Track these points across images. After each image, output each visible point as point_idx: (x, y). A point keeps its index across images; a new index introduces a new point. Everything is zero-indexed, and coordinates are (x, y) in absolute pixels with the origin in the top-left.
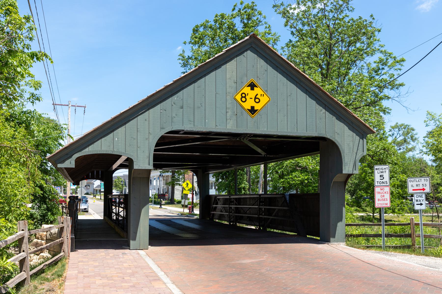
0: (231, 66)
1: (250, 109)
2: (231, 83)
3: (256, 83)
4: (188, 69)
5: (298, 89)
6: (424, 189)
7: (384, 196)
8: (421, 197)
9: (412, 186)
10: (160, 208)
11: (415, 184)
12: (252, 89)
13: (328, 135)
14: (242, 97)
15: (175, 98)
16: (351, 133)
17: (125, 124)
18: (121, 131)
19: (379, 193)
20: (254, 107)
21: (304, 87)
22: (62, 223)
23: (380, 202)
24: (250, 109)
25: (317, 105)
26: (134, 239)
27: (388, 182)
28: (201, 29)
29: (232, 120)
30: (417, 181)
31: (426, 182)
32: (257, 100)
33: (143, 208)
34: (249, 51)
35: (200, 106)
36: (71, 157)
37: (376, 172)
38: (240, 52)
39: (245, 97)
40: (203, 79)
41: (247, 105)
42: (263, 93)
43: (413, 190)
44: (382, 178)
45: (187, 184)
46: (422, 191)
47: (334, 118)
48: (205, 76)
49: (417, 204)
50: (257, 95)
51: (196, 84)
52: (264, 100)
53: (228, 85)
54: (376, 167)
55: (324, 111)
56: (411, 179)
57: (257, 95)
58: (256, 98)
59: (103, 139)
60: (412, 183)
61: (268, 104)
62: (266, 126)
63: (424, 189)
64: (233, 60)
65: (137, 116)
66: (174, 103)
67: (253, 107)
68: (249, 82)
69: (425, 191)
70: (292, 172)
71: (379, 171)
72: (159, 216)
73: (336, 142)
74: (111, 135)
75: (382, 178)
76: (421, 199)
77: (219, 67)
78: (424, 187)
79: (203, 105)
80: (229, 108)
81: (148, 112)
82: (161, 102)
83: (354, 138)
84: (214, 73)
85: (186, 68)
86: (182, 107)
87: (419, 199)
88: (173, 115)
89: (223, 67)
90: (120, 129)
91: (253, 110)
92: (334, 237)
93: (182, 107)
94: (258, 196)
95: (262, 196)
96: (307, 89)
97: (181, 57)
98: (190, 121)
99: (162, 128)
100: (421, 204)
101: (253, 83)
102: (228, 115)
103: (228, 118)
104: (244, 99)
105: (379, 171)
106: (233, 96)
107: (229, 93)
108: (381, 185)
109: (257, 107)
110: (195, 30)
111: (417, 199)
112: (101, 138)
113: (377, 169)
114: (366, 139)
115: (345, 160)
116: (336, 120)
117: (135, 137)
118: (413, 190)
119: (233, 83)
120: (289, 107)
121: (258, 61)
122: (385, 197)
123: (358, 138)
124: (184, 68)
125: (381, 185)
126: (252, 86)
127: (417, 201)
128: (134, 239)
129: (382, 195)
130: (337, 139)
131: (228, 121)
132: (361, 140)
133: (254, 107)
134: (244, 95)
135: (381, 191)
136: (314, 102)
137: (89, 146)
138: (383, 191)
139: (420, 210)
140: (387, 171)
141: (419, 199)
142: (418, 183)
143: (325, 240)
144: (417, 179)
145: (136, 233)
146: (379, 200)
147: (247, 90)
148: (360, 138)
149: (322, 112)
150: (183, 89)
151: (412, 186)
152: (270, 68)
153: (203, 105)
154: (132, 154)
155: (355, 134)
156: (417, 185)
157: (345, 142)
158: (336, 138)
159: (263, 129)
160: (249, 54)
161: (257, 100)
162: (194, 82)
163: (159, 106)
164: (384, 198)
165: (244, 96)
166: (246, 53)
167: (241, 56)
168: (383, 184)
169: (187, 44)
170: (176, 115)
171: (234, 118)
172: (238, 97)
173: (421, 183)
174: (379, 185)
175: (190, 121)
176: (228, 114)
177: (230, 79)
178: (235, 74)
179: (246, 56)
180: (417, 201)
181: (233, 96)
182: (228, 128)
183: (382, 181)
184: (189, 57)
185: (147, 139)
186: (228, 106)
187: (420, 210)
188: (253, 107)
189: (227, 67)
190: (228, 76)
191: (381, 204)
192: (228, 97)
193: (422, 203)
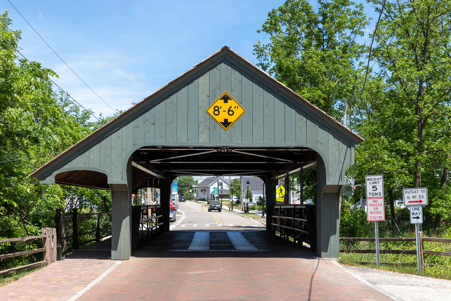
0: (203, 80)
2: (203, 97)
3: (229, 95)
5: (275, 98)
7: (377, 208)
8: (418, 209)
9: (408, 198)
10: (262, 217)
11: (411, 195)
12: (226, 102)
13: (309, 145)
14: (215, 110)
15: (147, 115)
17: (100, 142)
18: (96, 149)
19: (372, 205)
22: (45, 234)
23: (373, 215)
25: (297, 114)
26: (116, 249)
30: (414, 192)
31: (423, 194)
32: (231, 113)
33: (123, 220)
36: (51, 174)
37: (368, 182)
39: (218, 110)
40: (175, 95)
41: (220, 118)
43: (409, 202)
44: (375, 189)
45: (281, 190)
46: (419, 203)
47: (317, 126)
48: (177, 91)
49: (413, 218)
50: (231, 107)
51: (168, 100)
52: (238, 112)
53: (200, 100)
54: (368, 178)
55: (305, 119)
56: (407, 190)
57: (231, 107)
58: (229, 111)
60: (408, 195)
61: (243, 115)
62: (241, 138)
63: (421, 201)
64: (206, 75)
66: (146, 120)
67: (226, 120)
68: (222, 95)
69: (422, 203)
71: (371, 182)
72: (238, 227)
73: (318, 152)
75: (375, 189)
77: (192, 82)
78: (421, 199)
79: (175, 120)
81: (121, 130)
82: (133, 120)
83: (340, 147)
84: (186, 88)
86: (154, 124)
87: (415, 212)
90: (95, 147)
91: (226, 123)
92: (326, 251)
93: (154, 124)
94: (293, 207)
95: (297, 207)
98: (162, 137)
99: (135, 145)
102: (201, 128)
103: (200, 132)
104: (216, 113)
105: (371, 182)
106: (205, 110)
108: (374, 196)
109: (231, 119)
111: (414, 212)
112: (78, 156)
113: (368, 179)
114: (354, 147)
115: (328, 171)
116: (319, 129)
117: (109, 154)
118: (409, 202)
119: (206, 97)
120: (265, 118)
121: (232, 73)
122: (379, 210)
123: (345, 147)
125: (374, 196)
126: (226, 99)
127: (413, 214)
128: (116, 249)
129: (376, 207)
130: (320, 150)
131: (200, 135)
132: (349, 149)
134: (216, 108)
135: (374, 203)
137: (67, 163)
138: (376, 203)
139: (417, 224)
141: (415, 212)
142: (414, 195)
143: (314, 253)
145: (117, 244)
146: (371, 213)
147: (220, 103)
148: (348, 147)
149: (302, 122)
151: (408, 198)
152: (245, 79)
153: (175, 120)
154: (106, 170)
155: (341, 143)
156: (413, 197)
157: (329, 152)
159: (237, 142)
160: (223, 66)
161: (231, 113)
162: (166, 98)
163: (131, 124)
164: (377, 211)
165: (217, 110)
166: (219, 66)
167: (214, 70)
168: (376, 196)
170: (148, 131)
171: (207, 131)
172: (211, 111)
173: (417, 195)
174: (371, 196)
175: (162, 137)
176: (200, 128)
177: (202, 93)
178: (207, 88)
179: (219, 69)
180: (413, 214)
181: (205, 110)
182: (199, 142)
183: (374, 192)
186: (200, 120)
187: (417, 224)
188: (226, 120)
189: (200, 81)
190: (200, 90)
191: (375, 217)
192: (200, 112)
193: (419, 216)
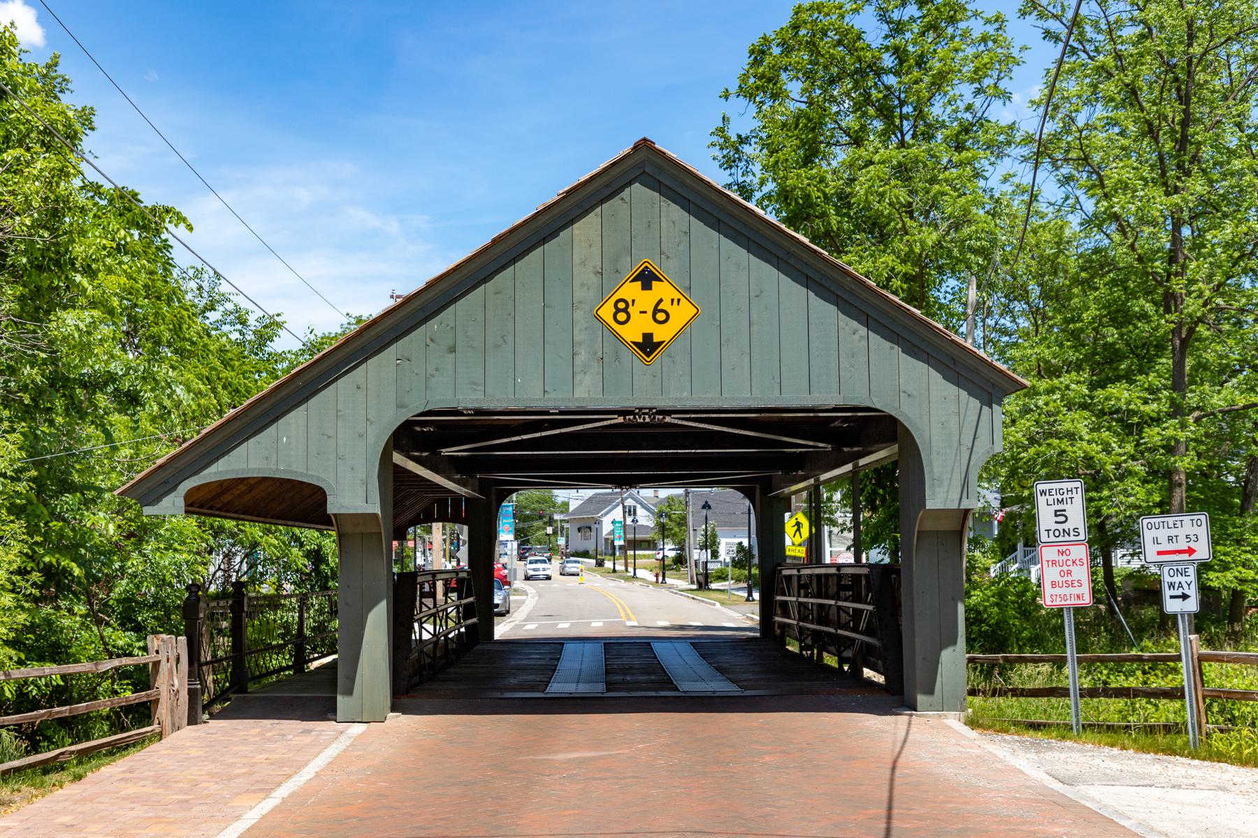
0: (586, 230)
1: (640, 340)
2: (584, 276)
3: (655, 267)
4: (740, 172)
6: (1191, 551)
7: (1069, 572)
8: (1184, 573)
9: (1156, 541)
11: (1162, 534)
12: (647, 286)
13: (875, 400)
14: (618, 310)
15: (434, 325)
16: (953, 389)
17: (306, 399)
18: (295, 418)
19: (1054, 563)
20: (651, 335)
21: (799, 271)
22: (157, 652)
23: (1057, 591)
24: (640, 340)
26: (349, 692)
27: (1082, 531)
28: (776, 51)
29: (588, 377)
30: (1171, 525)
31: (1196, 530)
32: (661, 316)
34: (637, 186)
35: (501, 342)
36: (174, 488)
37: (1041, 500)
38: (610, 190)
39: (625, 310)
40: (510, 270)
41: (632, 333)
42: (676, 295)
43: (1159, 553)
44: (1063, 519)
46: (1185, 557)
49: (1172, 597)
50: (661, 301)
51: (490, 286)
52: (682, 313)
53: (577, 282)
55: (863, 330)
56: (1152, 521)
57: (661, 301)
58: (656, 310)
59: (252, 441)
60: (1154, 533)
62: (688, 384)
63: (1191, 551)
64: (592, 214)
65: (337, 379)
66: (432, 340)
67: (648, 337)
68: (637, 268)
69: (1193, 557)
70: (229, 563)
72: (682, 628)
73: (901, 419)
74: (271, 430)
75: (1063, 519)
76: (1183, 579)
80: (580, 344)
82: (397, 339)
83: (963, 405)
85: (733, 170)
86: (453, 350)
87: (1177, 579)
88: (429, 371)
89: (564, 234)
91: (648, 345)
93: (453, 350)
95: (844, 571)
96: (810, 274)
97: (715, 139)
98: (475, 383)
99: (400, 406)
100: (1185, 597)
101: (651, 272)
102: (578, 360)
103: (577, 369)
107: (580, 302)
109: (661, 334)
110: (759, 54)
111: (1172, 580)
112: (247, 439)
113: (1043, 493)
115: (931, 472)
116: (903, 356)
118: (1159, 553)
119: (592, 275)
120: (754, 328)
121: (664, 209)
123: (975, 403)
124: (728, 171)
125: (1061, 539)
126: (646, 279)
128: (349, 692)
129: (1065, 568)
130: (907, 413)
131: (578, 378)
132: (985, 408)
133: (651, 335)
135: (1061, 558)
136: (833, 309)
138: (1065, 558)
140: (1078, 498)
141: (1177, 579)
142: (1173, 532)
144: (1171, 520)
146: (1054, 584)
147: (631, 290)
148: (982, 403)
149: (857, 337)
150: (455, 300)
151: (1156, 541)
152: (697, 226)
153: (510, 339)
154: (323, 476)
155: (964, 394)
156: (1170, 539)
158: (905, 409)
160: (637, 190)
161: (661, 316)
163: (392, 350)
164: (1070, 578)
165: (622, 308)
166: (627, 190)
167: (615, 201)
168: (1067, 538)
169: (732, 98)
170: (437, 369)
171: (596, 367)
172: (607, 312)
173: (1181, 532)
174: (1052, 539)
175: (475, 383)
178: (596, 250)
179: (627, 200)
180: (1171, 585)
183: (1060, 527)
184: (739, 136)
185: (361, 436)
188: (648, 337)
189: (576, 232)
191: (1064, 597)
193: (1187, 592)
